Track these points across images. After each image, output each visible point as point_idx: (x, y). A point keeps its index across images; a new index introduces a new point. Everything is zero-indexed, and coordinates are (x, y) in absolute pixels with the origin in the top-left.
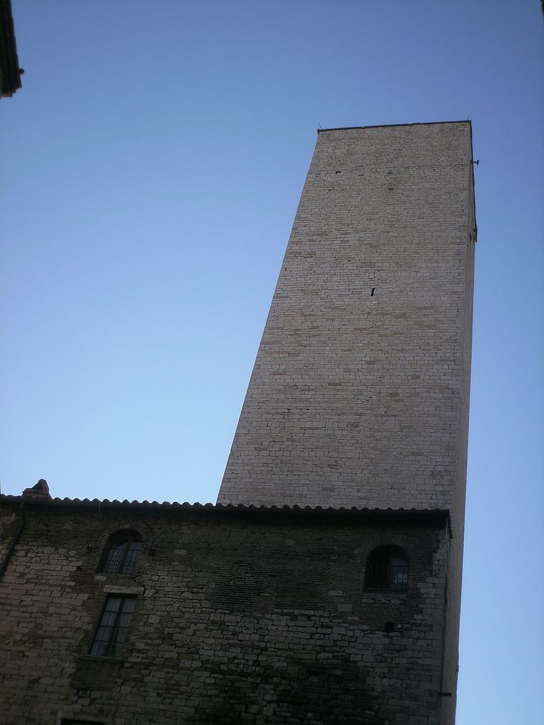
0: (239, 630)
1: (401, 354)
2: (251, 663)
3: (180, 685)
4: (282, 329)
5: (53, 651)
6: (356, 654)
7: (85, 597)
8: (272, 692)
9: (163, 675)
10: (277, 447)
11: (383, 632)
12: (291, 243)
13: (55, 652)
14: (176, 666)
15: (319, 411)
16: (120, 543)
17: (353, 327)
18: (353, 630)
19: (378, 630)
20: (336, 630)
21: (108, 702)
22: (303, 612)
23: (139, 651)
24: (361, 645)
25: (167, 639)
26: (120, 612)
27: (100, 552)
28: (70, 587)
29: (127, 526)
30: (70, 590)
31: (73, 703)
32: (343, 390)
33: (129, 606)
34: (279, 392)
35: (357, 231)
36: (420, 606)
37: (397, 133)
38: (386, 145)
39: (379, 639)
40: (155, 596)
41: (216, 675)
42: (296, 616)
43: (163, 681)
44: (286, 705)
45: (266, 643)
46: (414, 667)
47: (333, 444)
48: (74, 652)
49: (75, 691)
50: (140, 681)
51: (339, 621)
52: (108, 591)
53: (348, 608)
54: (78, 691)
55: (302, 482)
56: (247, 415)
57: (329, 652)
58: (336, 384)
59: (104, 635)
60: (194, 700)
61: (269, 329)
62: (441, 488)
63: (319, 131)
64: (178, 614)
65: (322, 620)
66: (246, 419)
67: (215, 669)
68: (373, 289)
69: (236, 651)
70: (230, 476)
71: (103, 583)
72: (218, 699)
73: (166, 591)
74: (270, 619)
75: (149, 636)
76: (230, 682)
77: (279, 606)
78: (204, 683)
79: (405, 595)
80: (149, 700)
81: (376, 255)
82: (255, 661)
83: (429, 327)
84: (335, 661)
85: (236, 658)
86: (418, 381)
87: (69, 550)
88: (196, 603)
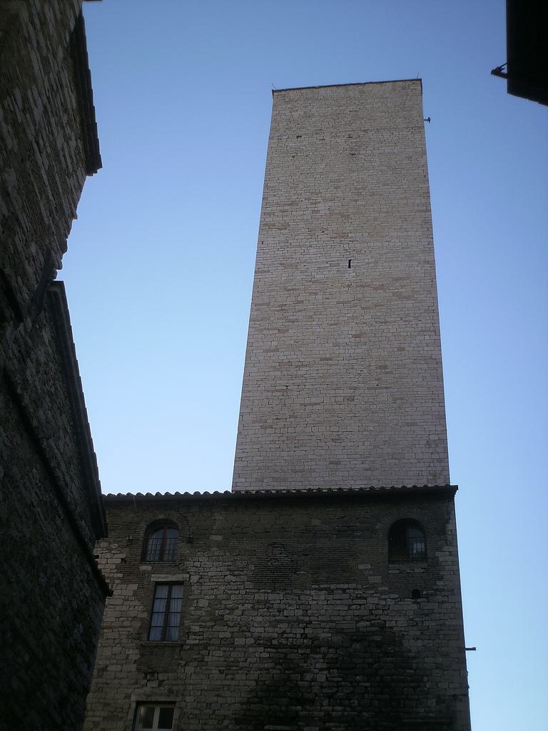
0: (282, 607)
1: (384, 327)
2: (298, 636)
3: (238, 662)
4: (268, 304)
5: (115, 639)
6: (391, 621)
7: (135, 587)
8: (322, 661)
10: (281, 424)
11: (412, 599)
12: (264, 214)
13: (117, 641)
15: (316, 386)
16: (156, 531)
17: (336, 300)
18: (385, 599)
19: (408, 598)
20: (370, 600)
21: (174, 682)
23: (195, 634)
24: (394, 612)
26: (169, 598)
27: (141, 543)
28: (119, 578)
29: (161, 517)
30: (119, 581)
31: (143, 686)
32: (335, 365)
33: (177, 592)
34: (275, 369)
35: (325, 200)
37: (351, 93)
38: (341, 106)
39: (409, 605)
40: (201, 581)
41: (269, 650)
42: (333, 591)
43: (221, 659)
44: (336, 671)
45: (310, 616)
46: (443, 628)
47: (332, 419)
48: (135, 639)
49: (143, 675)
51: (371, 592)
53: (377, 579)
56: (248, 394)
58: (327, 359)
59: (158, 620)
60: (253, 674)
61: (256, 306)
62: (437, 456)
63: (273, 91)
64: (224, 596)
66: (248, 398)
67: (268, 644)
68: (350, 261)
69: (284, 626)
72: (275, 672)
73: (211, 576)
74: (309, 595)
75: (202, 619)
76: (283, 655)
77: (316, 582)
78: (260, 658)
79: (426, 564)
80: (213, 677)
81: (347, 225)
82: (302, 634)
83: (408, 298)
84: (373, 629)
87: (110, 543)
88: (240, 585)
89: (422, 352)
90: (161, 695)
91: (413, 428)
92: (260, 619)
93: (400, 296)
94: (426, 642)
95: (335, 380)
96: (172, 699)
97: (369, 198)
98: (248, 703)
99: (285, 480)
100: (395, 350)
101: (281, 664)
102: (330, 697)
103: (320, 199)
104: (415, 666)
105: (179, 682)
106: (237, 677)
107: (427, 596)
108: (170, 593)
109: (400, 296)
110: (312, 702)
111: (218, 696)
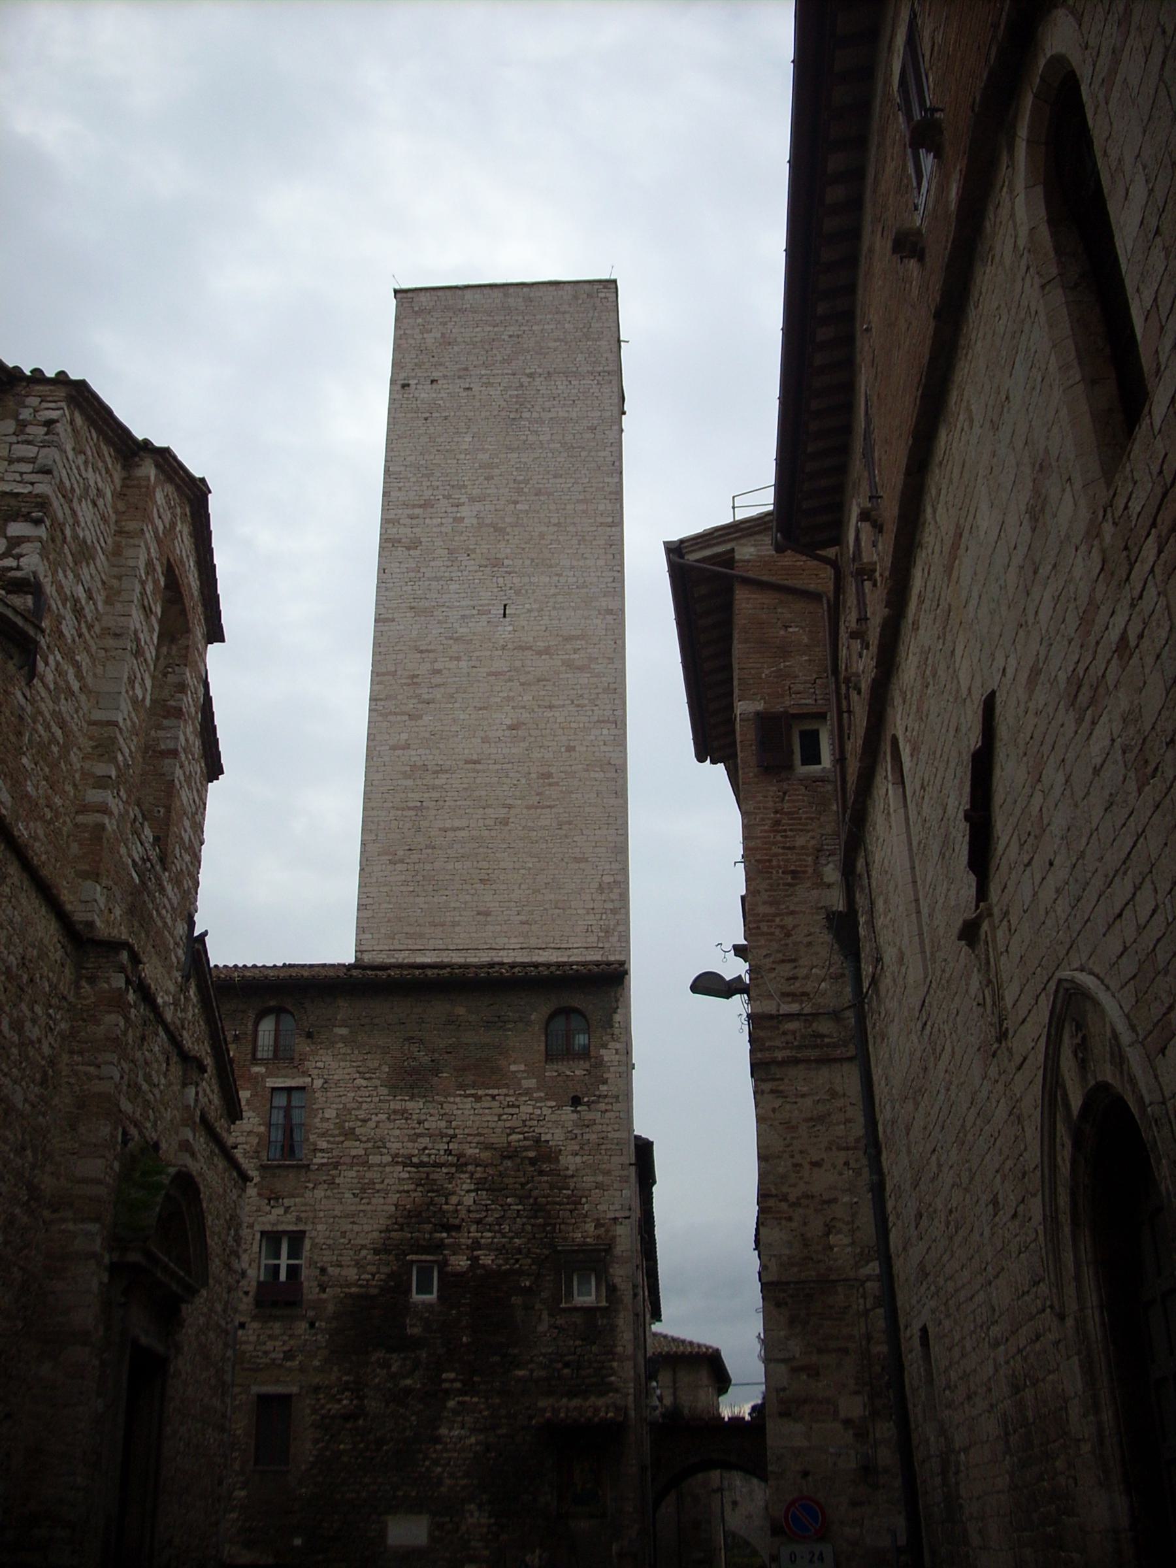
0: (423, 1117)
1: (548, 714)
2: (442, 1152)
3: (374, 1183)
4: (394, 674)
9: (353, 1174)
10: (415, 857)
14: (365, 1163)
18: (541, 1108)
20: (523, 1108)
21: (303, 1208)
22: (487, 1091)
23: (322, 1151)
25: (350, 1134)
33: (296, 1096)
34: (406, 776)
35: (472, 500)
36: (605, 1076)
38: (497, 325)
39: (567, 1114)
43: (356, 1181)
47: (481, 850)
50: (332, 1183)
52: (272, 1085)
53: (530, 1083)
54: (269, 1200)
55: (453, 905)
57: (520, 1133)
61: (377, 675)
62: (610, 905)
63: (396, 292)
64: (354, 1105)
65: (508, 1099)
67: (407, 1162)
69: (425, 1141)
70: (364, 902)
71: (264, 1077)
72: (416, 1194)
77: (461, 1086)
81: (503, 544)
83: (581, 669)
84: (527, 1143)
85: (425, 1148)
86: (573, 754)
89: (597, 754)
90: (289, 1223)
91: (582, 865)
92: (397, 1132)
93: (569, 665)
94: (585, 1158)
95: (483, 793)
96: (301, 1227)
97: (534, 498)
98: (388, 1230)
99: (421, 936)
100: (563, 749)
101: (422, 1185)
102: (479, 1222)
103: (464, 499)
104: (572, 1185)
105: (308, 1208)
106: (374, 1201)
107: (588, 1104)
108: (289, 1101)
109: (569, 665)
110: (458, 1228)
111: (353, 1223)
